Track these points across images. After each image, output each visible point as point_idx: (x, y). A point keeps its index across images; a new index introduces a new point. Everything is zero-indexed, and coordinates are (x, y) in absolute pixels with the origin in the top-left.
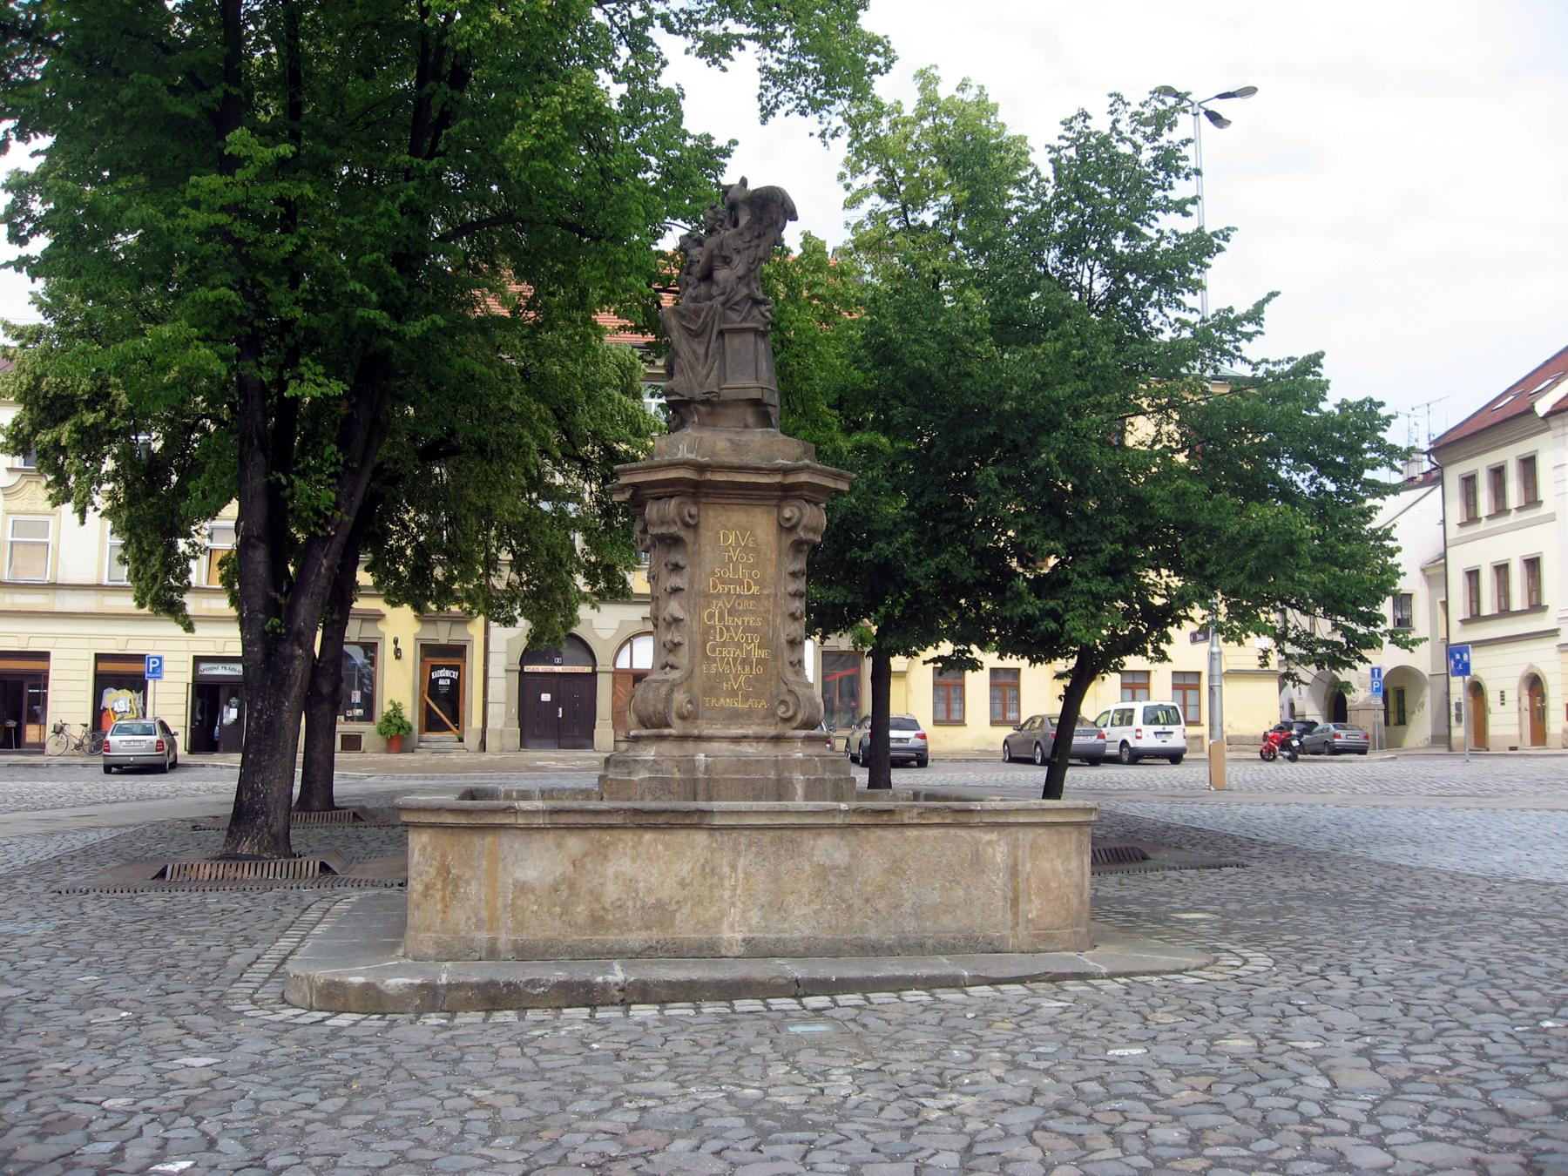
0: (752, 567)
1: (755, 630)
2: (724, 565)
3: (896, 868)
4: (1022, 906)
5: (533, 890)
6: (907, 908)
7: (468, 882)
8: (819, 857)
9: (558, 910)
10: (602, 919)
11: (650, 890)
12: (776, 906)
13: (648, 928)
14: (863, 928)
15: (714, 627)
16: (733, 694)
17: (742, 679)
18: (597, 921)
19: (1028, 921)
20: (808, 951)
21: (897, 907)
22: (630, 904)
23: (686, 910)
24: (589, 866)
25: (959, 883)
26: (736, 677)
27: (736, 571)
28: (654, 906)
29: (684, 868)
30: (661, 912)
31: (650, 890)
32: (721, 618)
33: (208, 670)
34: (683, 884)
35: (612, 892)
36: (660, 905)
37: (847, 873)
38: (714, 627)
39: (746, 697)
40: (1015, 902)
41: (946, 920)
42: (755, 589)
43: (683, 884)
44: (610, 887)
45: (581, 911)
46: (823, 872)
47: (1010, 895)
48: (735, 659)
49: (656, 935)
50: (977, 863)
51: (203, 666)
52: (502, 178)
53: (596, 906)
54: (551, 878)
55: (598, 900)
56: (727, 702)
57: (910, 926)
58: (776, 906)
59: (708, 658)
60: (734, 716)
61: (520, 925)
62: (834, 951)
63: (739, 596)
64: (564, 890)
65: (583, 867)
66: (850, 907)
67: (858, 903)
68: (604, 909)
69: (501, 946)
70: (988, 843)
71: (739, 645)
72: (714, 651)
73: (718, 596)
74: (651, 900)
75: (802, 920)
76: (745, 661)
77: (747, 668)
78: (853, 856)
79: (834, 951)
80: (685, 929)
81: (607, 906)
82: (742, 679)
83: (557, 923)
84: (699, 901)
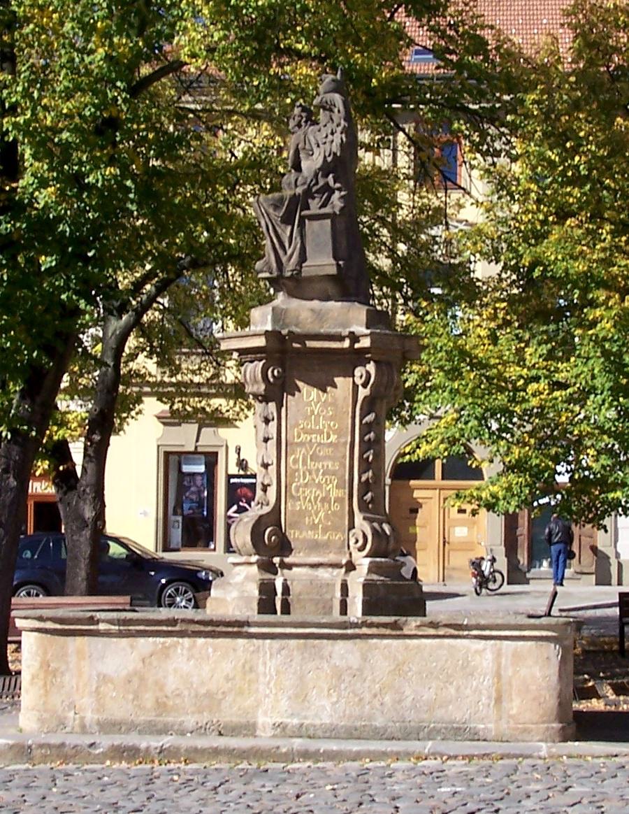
0: (332, 418)
1: (334, 473)
2: (307, 418)
3: (399, 669)
4: (504, 704)
5: (111, 681)
6: (408, 702)
7: (63, 674)
8: (336, 661)
9: (131, 697)
10: (165, 705)
11: (203, 683)
12: (301, 696)
13: (200, 712)
14: (370, 718)
15: (298, 470)
16: (314, 527)
17: (322, 514)
18: (161, 706)
19: (511, 717)
20: (332, 733)
21: (400, 702)
22: (186, 693)
23: (229, 698)
24: (155, 663)
25: (451, 683)
26: (317, 513)
27: (317, 423)
28: (205, 695)
29: (227, 667)
30: (211, 700)
31: (203, 683)
32: (305, 463)
33: (232, 481)
34: (228, 679)
35: (172, 683)
36: (209, 695)
37: (358, 674)
38: (298, 470)
39: (325, 530)
40: (499, 700)
41: (440, 713)
42: (333, 438)
43: (228, 679)
44: (171, 678)
45: (149, 699)
46: (338, 674)
47: (494, 695)
48: (316, 498)
49: (205, 718)
50: (468, 670)
51: (232, 481)
52: (569, 75)
53: (159, 694)
54: (124, 673)
55: (161, 690)
56: (310, 534)
57: (411, 716)
58: (301, 696)
59: (292, 497)
60: (315, 546)
61: (100, 707)
62: (352, 734)
63: (320, 444)
64: (135, 682)
65: (150, 664)
66: (361, 700)
67: (367, 697)
68: (166, 697)
69: (87, 722)
70: (476, 652)
71: (319, 486)
72: (297, 491)
73: (302, 444)
74: (203, 691)
75: (325, 710)
76: (325, 500)
77: (326, 506)
78: (365, 659)
79: (352, 734)
80: (229, 714)
81: (169, 694)
82: (322, 514)
83: (130, 706)
84: (241, 693)
